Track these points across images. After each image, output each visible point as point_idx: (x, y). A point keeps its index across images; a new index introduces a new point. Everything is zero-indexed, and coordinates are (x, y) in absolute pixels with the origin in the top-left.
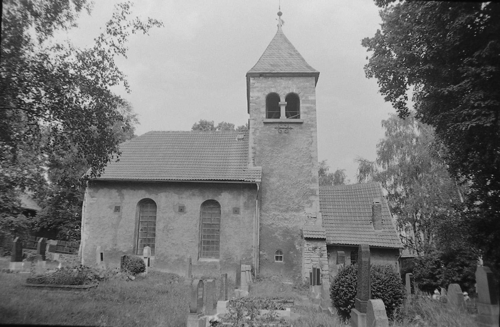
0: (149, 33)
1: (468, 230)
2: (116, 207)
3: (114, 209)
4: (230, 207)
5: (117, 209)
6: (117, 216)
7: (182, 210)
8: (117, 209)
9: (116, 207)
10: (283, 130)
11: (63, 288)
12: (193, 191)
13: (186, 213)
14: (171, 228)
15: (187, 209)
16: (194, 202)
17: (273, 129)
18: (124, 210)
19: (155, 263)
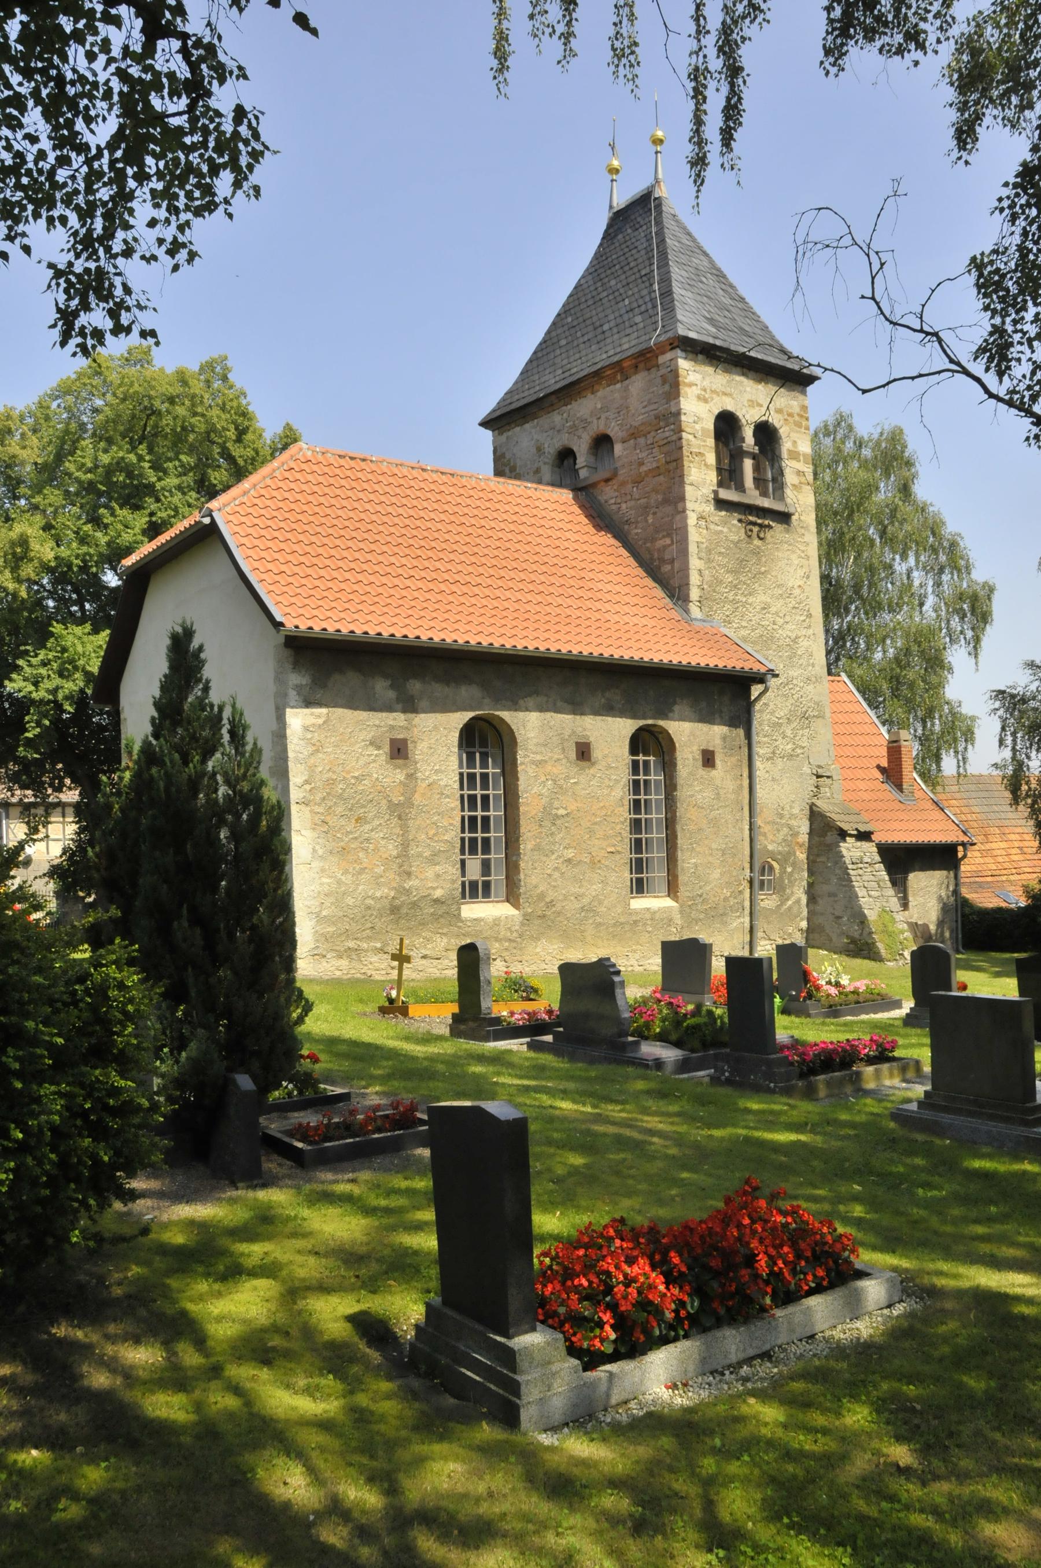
0: (254, 179)
1: (150, 398)
2: (393, 741)
3: (387, 748)
4: (695, 748)
5: (399, 750)
6: (400, 776)
7: (584, 752)
8: (399, 750)
9: (393, 741)
10: (756, 529)
11: (529, 1521)
12: (607, 694)
13: (593, 764)
14: (562, 812)
15: (596, 753)
16: (612, 733)
17: (735, 522)
18: (419, 751)
19: (522, 924)
